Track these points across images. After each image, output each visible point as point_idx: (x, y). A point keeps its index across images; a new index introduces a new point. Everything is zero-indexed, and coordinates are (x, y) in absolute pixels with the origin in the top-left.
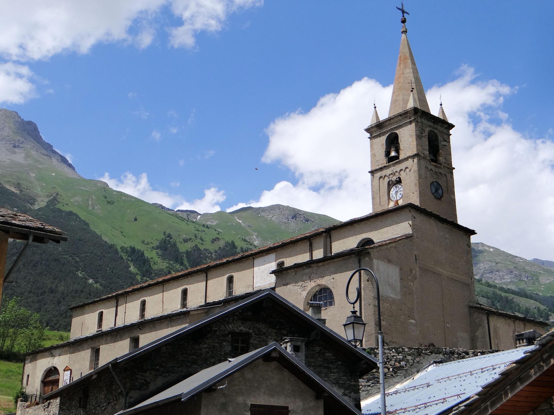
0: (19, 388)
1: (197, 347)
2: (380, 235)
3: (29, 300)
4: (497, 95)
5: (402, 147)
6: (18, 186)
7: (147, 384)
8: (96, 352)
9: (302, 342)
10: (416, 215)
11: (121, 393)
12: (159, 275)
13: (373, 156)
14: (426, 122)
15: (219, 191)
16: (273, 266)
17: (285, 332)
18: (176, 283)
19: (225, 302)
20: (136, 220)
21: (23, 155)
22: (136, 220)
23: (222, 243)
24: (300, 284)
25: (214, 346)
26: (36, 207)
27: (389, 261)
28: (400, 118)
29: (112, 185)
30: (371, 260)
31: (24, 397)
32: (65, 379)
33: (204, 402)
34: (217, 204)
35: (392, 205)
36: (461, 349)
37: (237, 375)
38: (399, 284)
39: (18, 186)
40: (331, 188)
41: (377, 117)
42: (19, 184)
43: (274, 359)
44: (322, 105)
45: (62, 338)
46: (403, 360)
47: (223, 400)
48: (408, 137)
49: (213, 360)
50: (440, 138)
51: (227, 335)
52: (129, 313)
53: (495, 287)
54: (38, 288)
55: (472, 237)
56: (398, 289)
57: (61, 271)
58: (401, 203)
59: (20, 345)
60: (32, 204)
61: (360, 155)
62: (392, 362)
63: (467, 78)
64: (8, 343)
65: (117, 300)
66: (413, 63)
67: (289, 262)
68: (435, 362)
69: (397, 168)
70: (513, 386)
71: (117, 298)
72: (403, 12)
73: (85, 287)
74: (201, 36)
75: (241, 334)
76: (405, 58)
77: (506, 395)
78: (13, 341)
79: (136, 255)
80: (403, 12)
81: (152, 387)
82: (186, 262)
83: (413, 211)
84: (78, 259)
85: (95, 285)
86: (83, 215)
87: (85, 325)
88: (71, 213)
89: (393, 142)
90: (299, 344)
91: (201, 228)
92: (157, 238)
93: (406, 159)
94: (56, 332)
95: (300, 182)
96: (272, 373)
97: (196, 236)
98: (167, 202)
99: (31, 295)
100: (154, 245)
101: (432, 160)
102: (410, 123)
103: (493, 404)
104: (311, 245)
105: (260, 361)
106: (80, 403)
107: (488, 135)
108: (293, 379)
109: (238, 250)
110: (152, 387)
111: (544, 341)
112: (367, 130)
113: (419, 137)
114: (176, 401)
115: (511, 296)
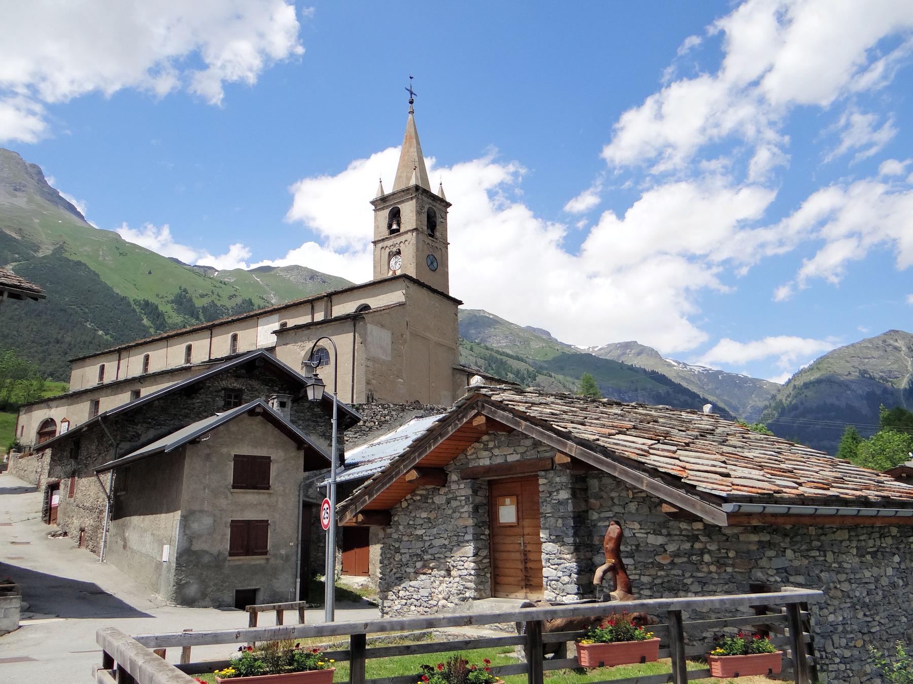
0: (13, 440)
1: (189, 402)
2: (376, 302)
3: (33, 350)
4: (515, 174)
5: (402, 221)
6: (20, 231)
7: (138, 436)
8: (96, 404)
9: (288, 398)
10: (411, 285)
11: (111, 445)
12: (172, 329)
13: (377, 227)
14: (425, 199)
15: (244, 248)
16: (276, 326)
17: (277, 389)
18: (180, 339)
19: (228, 359)
20: (150, 273)
21: (25, 199)
22: (150, 273)
23: (239, 300)
24: (299, 344)
25: (207, 401)
26: (40, 255)
27: (382, 326)
28: (404, 193)
29: (128, 235)
30: (366, 324)
31: (18, 448)
32: (62, 429)
33: (188, 453)
34: (242, 260)
35: (390, 274)
36: (440, 406)
37: (221, 428)
38: (390, 347)
39: (20, 231)
40: (355, 253)
41: (382, 191)
42: (20, 229)
43: (258, 414)
44: (355, 168)
45: (64, 389)
46: (388, 415)
47: (207, 451)
48: (409, 212)
49: (205, 414)
50: (438, 215)
51: (220, 391)
52: (132, 366)
53: (492, 350)
54: (42, 338)
55: (460, 307)
56: (389, 351)
57: (67, 321)
58: (398, 273)
59: (17, 395)
60: (35, 251)
61: (367, 224)
62: (378, 417)
63: (491, 157)
64: (4, 393)
65: (120, 353)
66: (418, 143)
67: (291, 323)
68: (416, 417)
69: (397, 240)
70: (436, 440)
71: (119, 351)
72: (412, 93)
73: (94, 338)
74: (231, 88)
75: (233, 390)
76: (411, 138)
77: (430, 447)
78: (10, 391)
79: (150, 308)
80: (412, 93)
81: (143, 439)
82: (201, 317)
83: (407, 281)
84: (87, 310)
85: (105, 337)
86: (92, 266)
87: (86, 376)
88: (79, 263)
89: (395, 215)
90: (285, 400)
91: (218, 285)
92: (172, 292)
93: (406, 232)
94: (57, 384)
95: (326, 244)
96: (256, 426)
97: (213, 293)
98: (186, 256)
99: (34, 344)
100: (169, 299)
101: (430, 235)
102: (412, 199)
103: (420, 455)
104: (313, 308)
105: (246, 415)
106: (71, 453)
107: (501, 208)
108: (277, 431)
109: (256, 307)
110: (143, 439)
111: (460, 404)
112: (373, 203)
113: (419, 213)
114: (160, 453)
115: (505, 358)
